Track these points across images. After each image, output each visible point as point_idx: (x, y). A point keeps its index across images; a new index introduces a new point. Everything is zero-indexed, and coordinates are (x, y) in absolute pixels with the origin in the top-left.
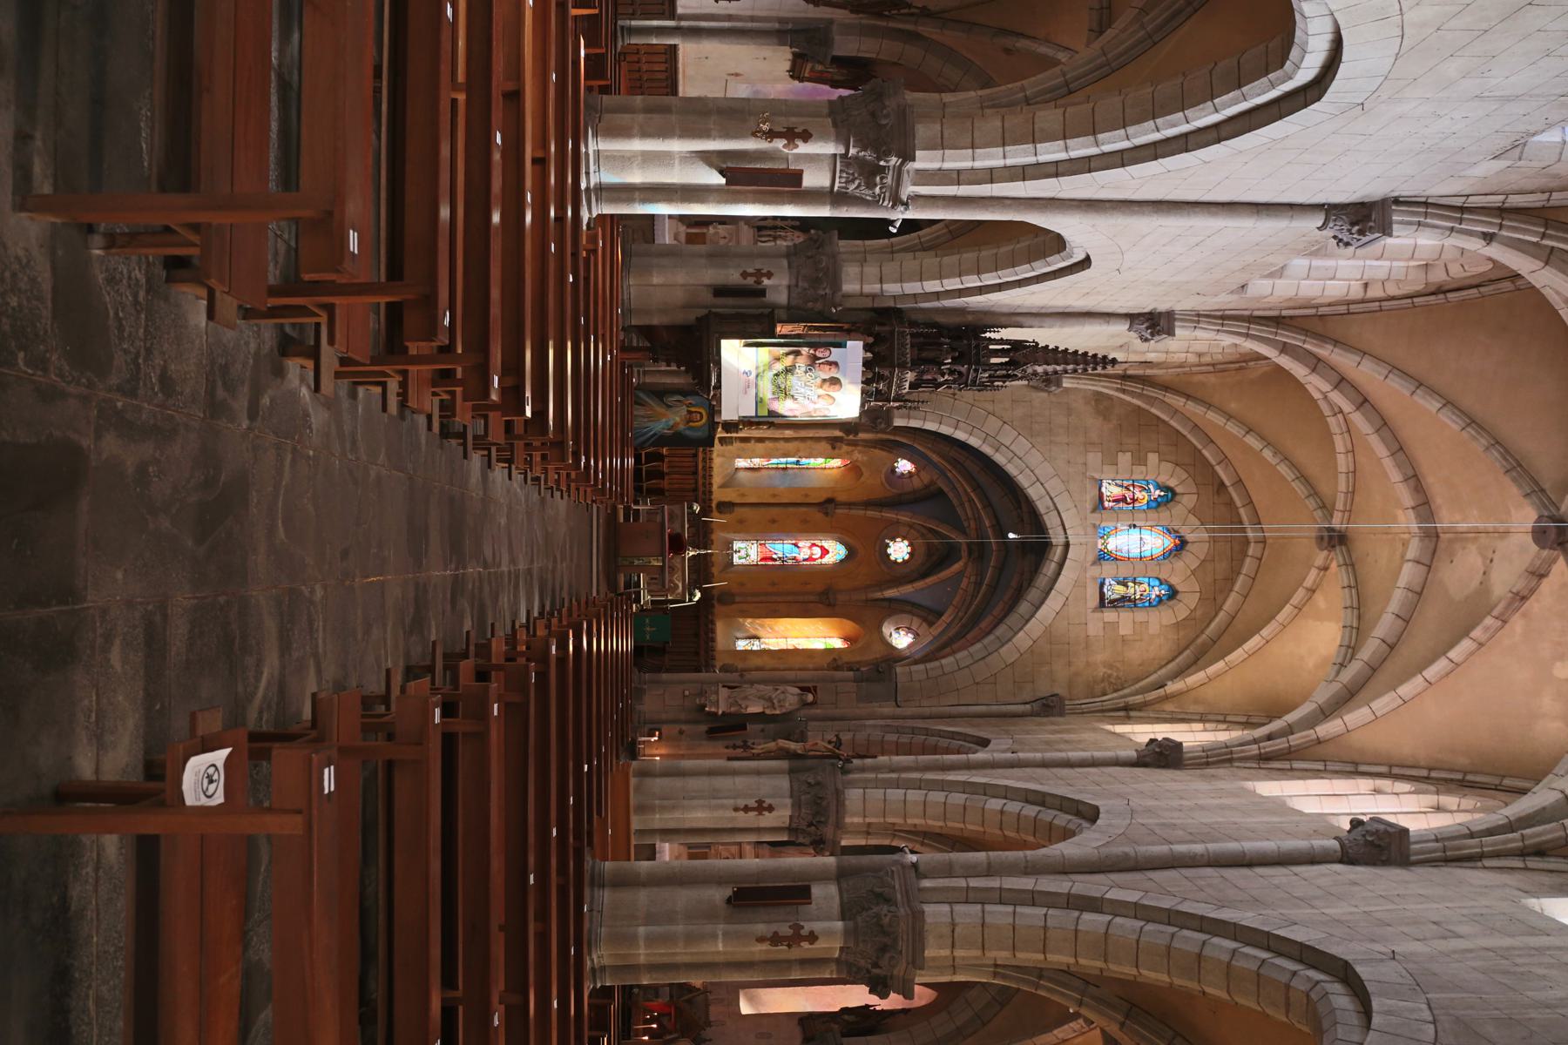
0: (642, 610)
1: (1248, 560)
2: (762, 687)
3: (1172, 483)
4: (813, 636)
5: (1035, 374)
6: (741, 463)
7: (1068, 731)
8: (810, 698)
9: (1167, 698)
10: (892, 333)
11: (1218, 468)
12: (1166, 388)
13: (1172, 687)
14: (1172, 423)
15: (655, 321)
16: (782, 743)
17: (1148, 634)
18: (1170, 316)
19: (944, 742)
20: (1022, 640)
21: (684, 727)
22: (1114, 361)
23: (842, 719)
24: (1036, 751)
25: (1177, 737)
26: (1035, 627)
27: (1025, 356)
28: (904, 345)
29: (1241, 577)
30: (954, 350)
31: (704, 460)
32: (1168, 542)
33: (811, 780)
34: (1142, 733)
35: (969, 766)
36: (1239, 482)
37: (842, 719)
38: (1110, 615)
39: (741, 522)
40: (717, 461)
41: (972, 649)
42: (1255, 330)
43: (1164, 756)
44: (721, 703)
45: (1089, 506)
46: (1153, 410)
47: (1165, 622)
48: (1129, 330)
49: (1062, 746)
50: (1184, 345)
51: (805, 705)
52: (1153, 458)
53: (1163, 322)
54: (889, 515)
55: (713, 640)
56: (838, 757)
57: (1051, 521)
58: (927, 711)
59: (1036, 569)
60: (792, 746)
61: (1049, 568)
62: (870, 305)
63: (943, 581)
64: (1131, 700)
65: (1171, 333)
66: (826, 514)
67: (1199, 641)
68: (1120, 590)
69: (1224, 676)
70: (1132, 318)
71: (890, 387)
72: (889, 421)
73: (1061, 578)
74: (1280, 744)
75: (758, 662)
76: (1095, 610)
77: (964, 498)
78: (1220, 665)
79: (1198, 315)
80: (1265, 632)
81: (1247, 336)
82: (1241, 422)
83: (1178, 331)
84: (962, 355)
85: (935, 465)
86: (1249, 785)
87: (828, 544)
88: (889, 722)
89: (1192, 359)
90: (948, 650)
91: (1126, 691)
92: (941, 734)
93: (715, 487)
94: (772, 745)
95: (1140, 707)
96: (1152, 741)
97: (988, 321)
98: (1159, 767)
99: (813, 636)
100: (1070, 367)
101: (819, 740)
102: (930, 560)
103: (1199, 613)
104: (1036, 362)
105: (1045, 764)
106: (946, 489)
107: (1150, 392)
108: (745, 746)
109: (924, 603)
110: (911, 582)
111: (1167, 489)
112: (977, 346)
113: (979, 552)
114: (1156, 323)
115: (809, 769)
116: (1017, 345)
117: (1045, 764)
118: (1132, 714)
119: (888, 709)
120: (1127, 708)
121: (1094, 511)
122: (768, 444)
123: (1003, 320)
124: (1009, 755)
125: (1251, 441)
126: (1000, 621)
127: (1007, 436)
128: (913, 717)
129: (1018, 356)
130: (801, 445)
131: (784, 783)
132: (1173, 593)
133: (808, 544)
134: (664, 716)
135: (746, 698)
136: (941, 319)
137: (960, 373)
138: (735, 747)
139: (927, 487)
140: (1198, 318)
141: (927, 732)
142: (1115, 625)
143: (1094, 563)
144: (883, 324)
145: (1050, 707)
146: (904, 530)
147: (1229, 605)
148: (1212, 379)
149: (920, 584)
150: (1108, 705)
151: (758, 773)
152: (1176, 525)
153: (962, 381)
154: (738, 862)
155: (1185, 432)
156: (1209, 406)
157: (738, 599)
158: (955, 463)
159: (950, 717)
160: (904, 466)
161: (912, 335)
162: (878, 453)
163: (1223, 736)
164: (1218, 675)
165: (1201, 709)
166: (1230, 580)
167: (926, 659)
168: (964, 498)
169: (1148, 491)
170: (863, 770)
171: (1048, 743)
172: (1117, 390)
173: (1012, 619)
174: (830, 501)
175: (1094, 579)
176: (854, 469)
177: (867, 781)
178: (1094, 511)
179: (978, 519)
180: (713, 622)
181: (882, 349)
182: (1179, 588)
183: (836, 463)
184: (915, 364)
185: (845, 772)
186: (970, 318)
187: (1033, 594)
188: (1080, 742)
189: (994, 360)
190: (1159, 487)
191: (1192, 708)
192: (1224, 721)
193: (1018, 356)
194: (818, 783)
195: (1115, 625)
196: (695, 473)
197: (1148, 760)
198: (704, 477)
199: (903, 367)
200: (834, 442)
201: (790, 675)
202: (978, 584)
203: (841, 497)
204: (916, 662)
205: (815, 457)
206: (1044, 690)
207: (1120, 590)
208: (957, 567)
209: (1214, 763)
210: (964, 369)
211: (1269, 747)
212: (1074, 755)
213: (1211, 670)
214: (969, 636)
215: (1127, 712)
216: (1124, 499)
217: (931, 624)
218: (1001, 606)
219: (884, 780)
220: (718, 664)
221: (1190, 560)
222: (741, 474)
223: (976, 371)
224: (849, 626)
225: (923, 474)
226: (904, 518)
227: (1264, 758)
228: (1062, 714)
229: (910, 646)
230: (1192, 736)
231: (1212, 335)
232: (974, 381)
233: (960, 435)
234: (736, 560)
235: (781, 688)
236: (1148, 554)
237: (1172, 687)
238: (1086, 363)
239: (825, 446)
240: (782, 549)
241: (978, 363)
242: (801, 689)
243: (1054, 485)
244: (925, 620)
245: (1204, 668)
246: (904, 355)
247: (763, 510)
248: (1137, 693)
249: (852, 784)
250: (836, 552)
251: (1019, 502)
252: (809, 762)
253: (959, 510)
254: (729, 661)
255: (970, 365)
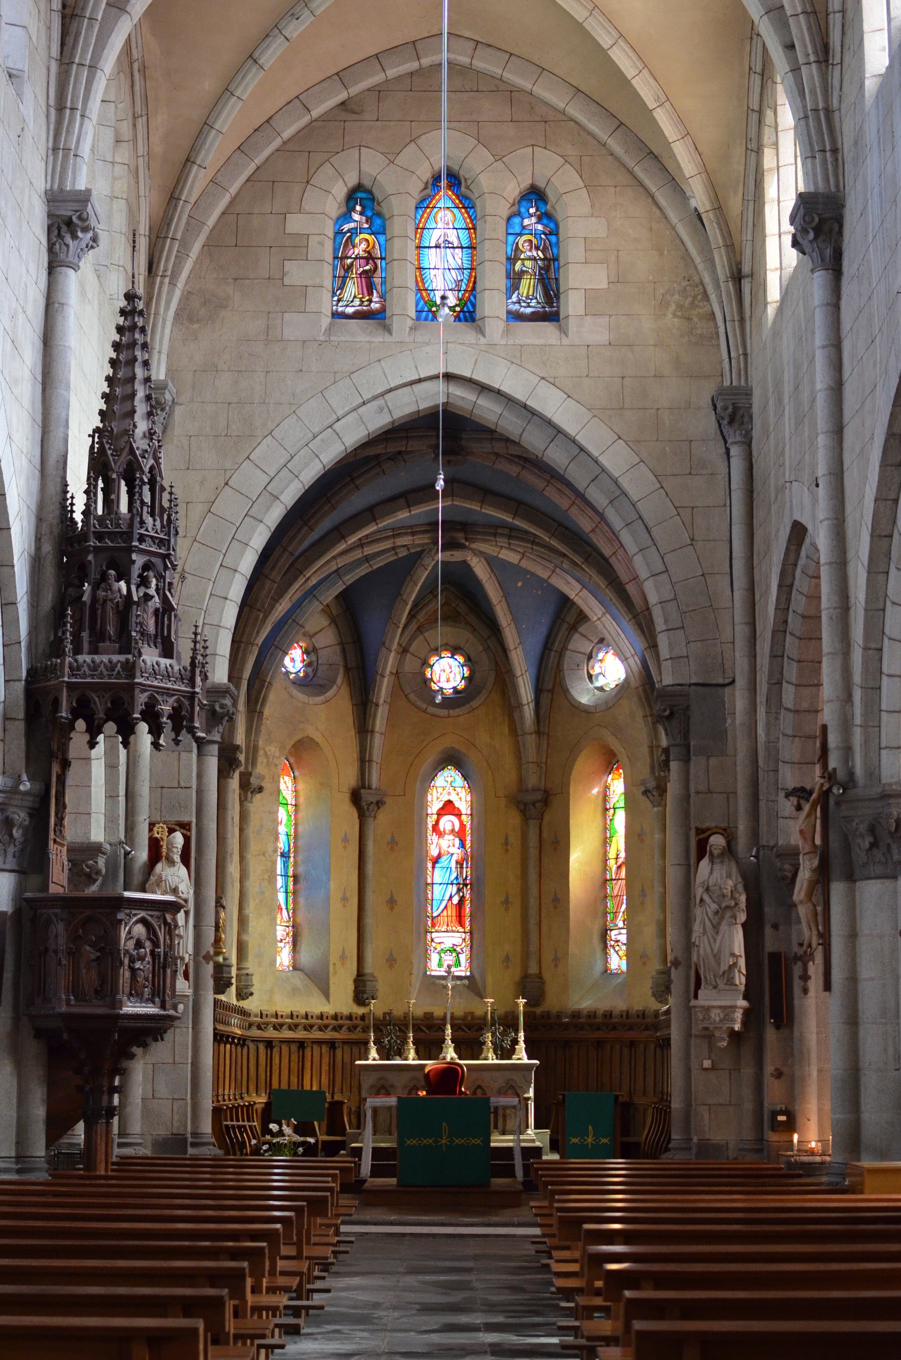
0: (555, 1146)
1: (478, 64)
2: (697, 928)
3: (340, 191)
4: (601, 827)
5: (150, 434)
6: (284, 958)
7: (778, 383)
8: (717, 841)
9: (719, 208)
10: (71, 686)
11: (315, 113)
12: (172, 198)
13: (700, 199)
14: (233, 190)
15: (40, 1112)
16: (799, 892)
17: (602, 243)
18: (53, 198)
19: (799, 603)
20: (616, 459)
21: (769, 1069)
22: (130, 297)
23: (754, 782)
24: (812, 442)
25: (789, 203)
26: (594, 436)
27: (117, 452)
28: (94, 667)
29: (507, 75)
30: (104, 577)
31: (278, 1027)
32: (444, 199)
33: (867, 842)
34: (780, 256)
35: (841, 564)
36: (341, 77)
37: (754, 782)
38: (573, 304)
39: (391, 961)
40: (284, 1005)
41: (631, 548)
42: (83, 54)
43: (821, 223)
44: (727, 1004)
45: (379, 338)
46: (211, 221)
47: (587, 209)
48: (76, 268)
49: (805, 396)
50: (102, 173)
51: (730, 850)
52: (296, 224)
53: (65, 211)
54: (384, 689)
55: (608, 1015)
56: (825, 795)
57: (405, 405)
58: (741, 631)
59: (488, 433)
60: (805, 875)
61: (488, 411)
62: (21, 725)
63: (506, 596)
64: (722, 270)
65: (84, 198)
66: (379, 804)
67: (618, 150)
68: (527, 285)
69: (681, 113)
70: (55, 264)
71: (168, 692)
72: (217, 692)
73: (505, 388)
74: (800, 30)
75: (650, 932)
76: (564, 331)
77: (358, 554)
78: (662, 117)
79: (55, 149)
80: (605, 40)
81: (93, 67)
82: (236, 73)
83: (81, 185)
84: (112, 564)
85: (297, 606)
86: (871, 85)
87: (434, 806)
88: (761, 698)
89: (124, 154)
90: (631, 589)
91: (707, 279)
92: (783, 607)
93: (329, 1009)
94: (803, 911)
95: (731, 247)
96: (795, 244)
97: (53, 515)
98: (840, 233)
99: (601, 827)
100: (139, 372)
101: (793, 828)
102: (465, 610)
103: (570, 151)
104: (128, 433)
105: (838, 431)
106: (339, 587)
107: (178, 227)
108: (805, 959)
109: (543, 630)
110: (505, 651)
111: (351, 198)
112: (99, 536)
113: (459, 531)
114: (66, 224)
115: (847, 847)
116: (98, 465)
117: (838, 431)
118: (746, 269)
119: (739, 700)
120: (737, 277)
121: (388, 329)
122: (251, 910)
123: (53, 488)
124: (822, 492)
125: (270, 56)
126: (581, 496)
127: (249, 478)
128: (753, 656)
129: (118, 465)
130: (253, 847)
131: (871, 891)
132: (535, 194)
133: (432, 838)
134: (748, 1106)
135: (717, 957)
136: (48, 598)
137: (146, 567)
138: (805, 977)
139: (333, 621)
140: (60, 149)
141: (781, 630)
142: (591, 296)
143: (481, 331)
144: (56, 703)
145: (734, 412)
146: (410, 665)
147: (557, 98)
148: (160, 120)
149: (510, 635)
150: (731, 310)
151: (853, 936)
152: (415, 187)
153: (165, 559)
154: (22, 644)
155: (252, 167)
156: (206, 125)
157: (533, 969)
158: (295, 571)
159: (751, 588)
160: (294, 661)
161: (77, 651)
162: (271, 710)
163: (786, 116)
164: (680, 120)
165: (739, 151)
166: (512, 94)
167: (642, 621)
168: (358, 554)
169: (354, 232)
170: (847, 750)
171: (799, 421)
172: (173, 284)
173: (578, 476)
174: (356, 797)
175: (507, 332)
176: (301, 752)
177: (866, 743)
178: (388, 329)
179: (397, 531)
180: (576, 1015)
181: (100, 705)
182: (526, 183)
183: (286, 785)
184: (126, 645)
185: (849, 782)
186: (47, 548)
187: (534, 440)
188: (797, 366)
189: (124, 508)
190: (346, 216)
191: (737, 166)
192: (760, 112)
193: (118, 465)
194: (872, 830)
195: (591, 296)
196: (301, 1044)
197: (828, 252)
198: (308, 1028)
199: (130, 669)
200: (248, 788)
201: (674, 875)
202: (513, 534)
203: (349, 777)
204: (653, 646)
205: (276, 822)
206: (705, 423)
207: (527, 285)
208: (480, 570)
209: (833, 140)
210: (139, 560)
211: (805, 47)
212: (821, 379)
213: (670, 130)
214: (607, 551)
215: (743, 275)
216: (368, 277)
217: (582, 617)
218: (552, 493)
219: (866, 714)
220: (653, 1005)
221: (479, 166)
222: (305, 958)
223: (142, 539)
224: (584, 764)
225: (310, 627)
226: (389, 662)
227: (824, 55)
228: (747, 393)
229: (621, 655)
230: (785, 180)
231: (90, 128)
232: (161, 543)
233: (247, 563)
234: (462, 970)
235: (699, 892)
236: (463, 235)
237: (700, 199)
238: (133, 344)
239: (257, 803)
240: (443, 886)
241: (128, 536)
242: (700, 857)
243: (340, 398)
244: (574, 628)
245: (667, 144)
246: (111, 666)
247: (369, 921)
248: (710, 262)
249: (873, 774)
250: (449, 787)
251: (368, 460)
252: (835, 844)
253: (378, 563)
254: (647, 987)
255: (130, 550)
